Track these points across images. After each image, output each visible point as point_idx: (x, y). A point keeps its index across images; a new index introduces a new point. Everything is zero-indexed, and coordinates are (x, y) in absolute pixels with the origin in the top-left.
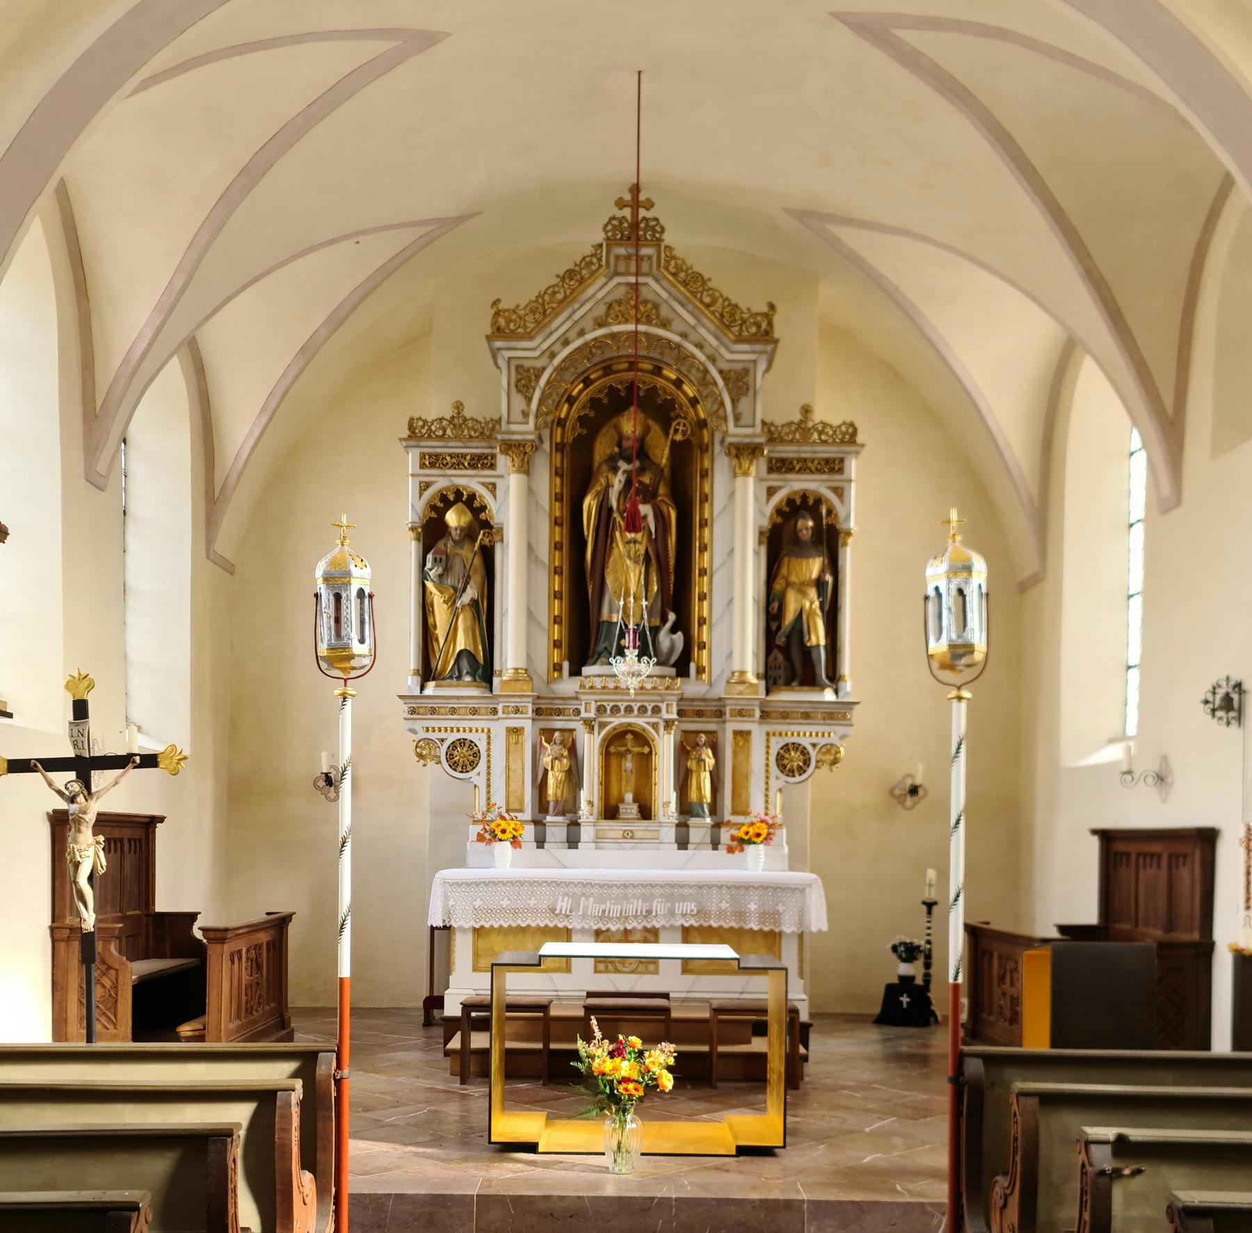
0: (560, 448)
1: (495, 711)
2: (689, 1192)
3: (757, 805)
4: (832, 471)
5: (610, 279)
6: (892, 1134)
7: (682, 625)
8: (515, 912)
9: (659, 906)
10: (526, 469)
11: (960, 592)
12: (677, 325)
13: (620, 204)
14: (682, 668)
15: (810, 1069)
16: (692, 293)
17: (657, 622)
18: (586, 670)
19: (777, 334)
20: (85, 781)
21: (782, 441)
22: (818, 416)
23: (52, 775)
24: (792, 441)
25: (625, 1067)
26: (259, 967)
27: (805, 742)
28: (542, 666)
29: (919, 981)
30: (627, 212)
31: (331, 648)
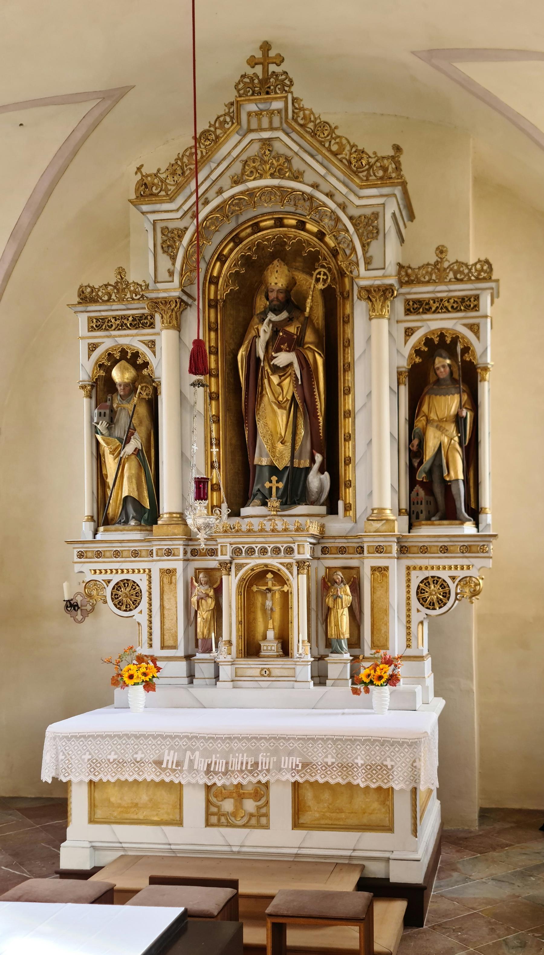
4: (468, 308)
5: (244, 136)
7: (331, 465)
12: (309, 177)
13: (252, 62)
16: (321, 142)
18: (245, 511)
22: (451, 257)
24: (428, 282)
27: (444, 575)
30: (259, 70)
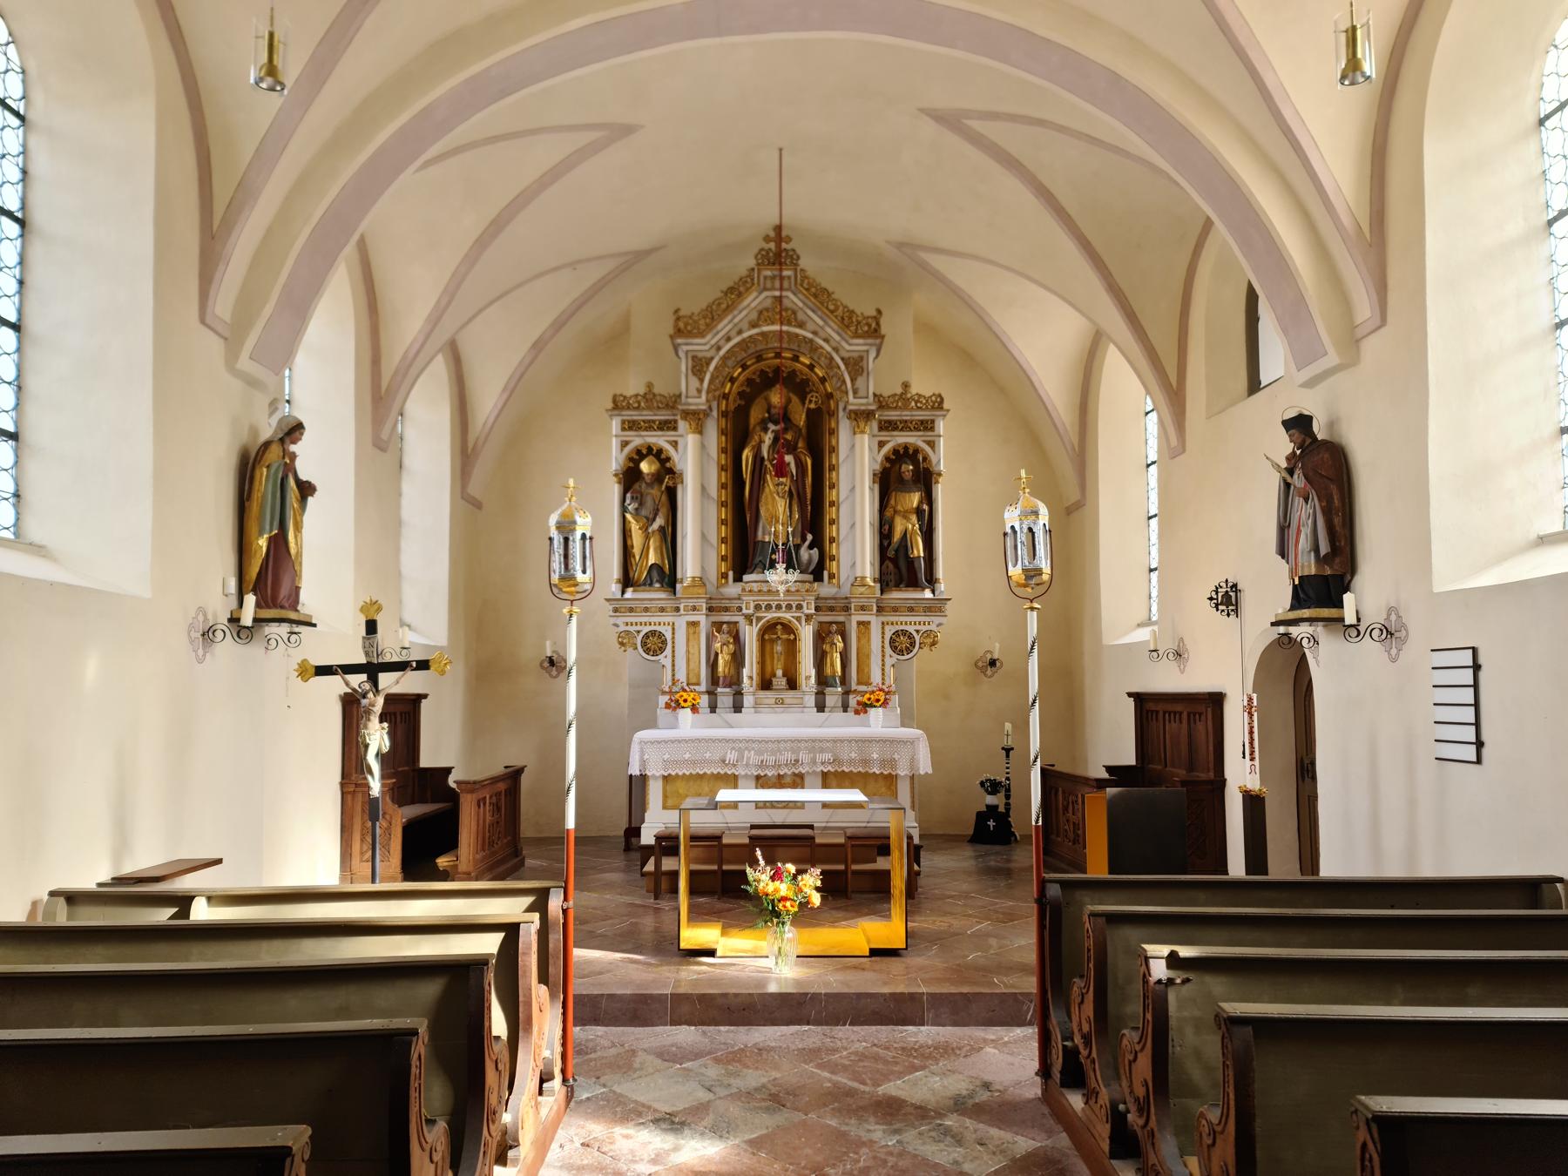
0: (724, 414)
1: (678, 609)
2: (836, 988)
3: (876, 677)
4: (926, 429)
6: (988, 935)
7: (817, 543)
8: (694, 763)
9: (804, 756)
10: (700, 430)
11: (1030, 530)
12: (810, 326)
13: (767, 239)
14: (817, 575)
15: (922, 881)
17: (798, 541)
18: (746, 578)
19: (883, 331)
20: (374, 680)
21: (888, 407)
22: (914, 390)
23: (349, 677)
25: (784, 888)
26: (499, 809)
27: (911, 629)
28: (713, 575)
29: (1002, 809)
30: (772, 245)
31: (562, 578)
